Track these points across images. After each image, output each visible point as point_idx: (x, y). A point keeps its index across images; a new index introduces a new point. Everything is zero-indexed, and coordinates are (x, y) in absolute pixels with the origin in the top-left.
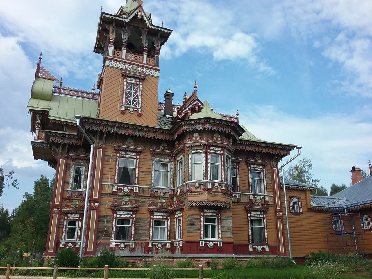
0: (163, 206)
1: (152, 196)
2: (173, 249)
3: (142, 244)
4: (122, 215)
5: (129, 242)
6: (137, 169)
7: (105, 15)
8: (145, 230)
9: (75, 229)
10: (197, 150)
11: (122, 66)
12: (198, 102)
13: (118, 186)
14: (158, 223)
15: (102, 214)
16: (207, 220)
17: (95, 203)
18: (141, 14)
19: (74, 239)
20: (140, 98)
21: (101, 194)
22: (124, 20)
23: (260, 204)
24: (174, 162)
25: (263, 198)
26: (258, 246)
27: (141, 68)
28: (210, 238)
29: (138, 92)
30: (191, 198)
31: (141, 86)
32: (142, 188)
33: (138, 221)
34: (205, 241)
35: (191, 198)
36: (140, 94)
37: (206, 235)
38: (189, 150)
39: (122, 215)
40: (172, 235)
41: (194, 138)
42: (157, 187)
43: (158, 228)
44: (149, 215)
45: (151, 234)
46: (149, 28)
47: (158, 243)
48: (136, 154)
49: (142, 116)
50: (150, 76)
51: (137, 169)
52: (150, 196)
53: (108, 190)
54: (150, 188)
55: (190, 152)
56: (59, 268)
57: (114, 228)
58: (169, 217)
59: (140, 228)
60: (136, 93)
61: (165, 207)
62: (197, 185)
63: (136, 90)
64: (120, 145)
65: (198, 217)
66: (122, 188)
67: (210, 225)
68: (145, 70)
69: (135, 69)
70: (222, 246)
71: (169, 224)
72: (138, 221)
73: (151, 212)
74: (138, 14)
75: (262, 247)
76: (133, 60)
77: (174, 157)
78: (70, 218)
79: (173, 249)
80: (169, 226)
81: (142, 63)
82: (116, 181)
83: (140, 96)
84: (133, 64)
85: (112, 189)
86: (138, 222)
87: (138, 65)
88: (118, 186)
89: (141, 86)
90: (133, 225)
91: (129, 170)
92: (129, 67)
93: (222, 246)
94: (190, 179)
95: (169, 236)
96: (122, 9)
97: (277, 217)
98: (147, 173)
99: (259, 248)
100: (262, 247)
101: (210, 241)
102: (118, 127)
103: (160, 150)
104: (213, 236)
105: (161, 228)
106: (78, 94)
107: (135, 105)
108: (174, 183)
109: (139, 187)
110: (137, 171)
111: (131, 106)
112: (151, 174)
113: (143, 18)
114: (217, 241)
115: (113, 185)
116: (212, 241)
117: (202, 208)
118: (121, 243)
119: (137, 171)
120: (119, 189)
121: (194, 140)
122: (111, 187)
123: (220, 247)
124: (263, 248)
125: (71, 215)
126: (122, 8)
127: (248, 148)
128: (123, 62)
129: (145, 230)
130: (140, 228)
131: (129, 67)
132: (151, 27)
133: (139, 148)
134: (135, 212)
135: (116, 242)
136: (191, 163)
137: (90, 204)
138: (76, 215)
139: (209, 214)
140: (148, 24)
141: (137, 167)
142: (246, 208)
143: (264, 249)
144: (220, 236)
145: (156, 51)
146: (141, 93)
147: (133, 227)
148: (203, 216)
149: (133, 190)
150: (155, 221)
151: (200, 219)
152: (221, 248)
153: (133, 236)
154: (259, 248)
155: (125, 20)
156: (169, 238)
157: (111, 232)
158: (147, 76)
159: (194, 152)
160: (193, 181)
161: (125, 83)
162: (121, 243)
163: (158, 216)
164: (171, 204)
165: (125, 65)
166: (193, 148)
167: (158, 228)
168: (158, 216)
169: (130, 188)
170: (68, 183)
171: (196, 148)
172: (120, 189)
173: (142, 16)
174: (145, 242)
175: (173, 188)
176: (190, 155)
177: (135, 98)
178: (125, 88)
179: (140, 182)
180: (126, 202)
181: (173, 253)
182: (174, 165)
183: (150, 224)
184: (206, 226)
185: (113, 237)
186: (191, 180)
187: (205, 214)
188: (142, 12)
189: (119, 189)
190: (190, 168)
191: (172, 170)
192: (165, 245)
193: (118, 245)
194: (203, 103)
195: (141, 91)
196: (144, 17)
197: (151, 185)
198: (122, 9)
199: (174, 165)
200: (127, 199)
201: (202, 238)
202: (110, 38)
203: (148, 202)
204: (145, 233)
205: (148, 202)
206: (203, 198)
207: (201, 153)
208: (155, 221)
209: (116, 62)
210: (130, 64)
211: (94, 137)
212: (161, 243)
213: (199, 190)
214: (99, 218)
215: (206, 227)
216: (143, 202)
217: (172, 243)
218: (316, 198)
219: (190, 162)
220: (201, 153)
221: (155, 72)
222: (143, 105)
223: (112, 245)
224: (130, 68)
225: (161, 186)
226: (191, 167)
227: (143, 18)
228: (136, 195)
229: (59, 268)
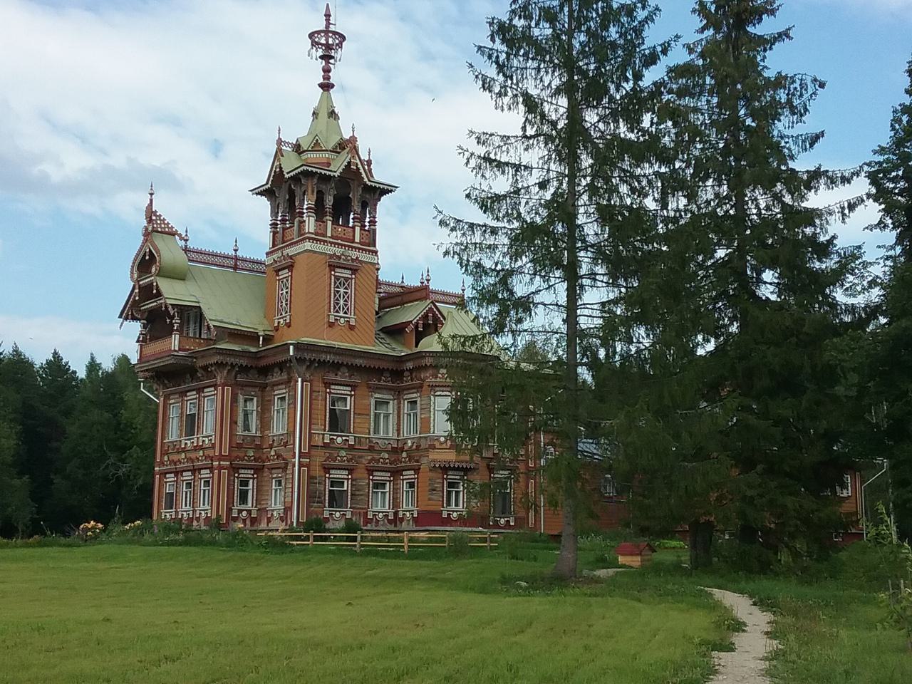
1: (371, 449)
2: (396, 520)
3: (360, 513)
4: (337, 474)
5: (345, 511)
6: (352, 410)
8: (361, 495)
9: (247, 491)
10: (443, 391)
11: (330, 250)
12: (433, 307)
13: (330, 435)
14: (376, 486)
15: (313, 473)
16: (451, 485)
19: (247, 505)
21: (311, 447)
22: (332, 174)
23: (508, 460)
24: (398, 399)
25: (347, 321)
26: (501, 518)
28: (453, 507)
29: (349, 291)
30: (433, 455)
31: (353, 281)
32: (358, 437)
33: (354, 483)
34: (448, 511)
35: (433, 455)
37: (449, 504)
38: (431, 390)
39: (337, 474)
40: (396, 503)
41: (440, 375)
42: (376, 436)
43: (377, 492)
44: (367, 476)
45: (370, 500)
46: (365, 184)
47: (379, 512)
48: (350, 389)
49: (356, 330)
51: (352, 410)
52: (369, 449)
53: (318, 441)
54: (369, 438)
55: (432, 393)
56: (315, 534)
57: (327, 493)
58: (392, 479)
59: (357, 493)
60: (346, 293)
61: (388, 465)
62: (442, 439)
63: (346, 288)
64: (331, 377)
65: (440, 481)
66: (335, 437)
71: (392, 487)
72: (354, 483)
73: (370, 471)
75: (506, 519)
77: (399, 392)
78: (242, 476)
79: (396, 520)
80: (392, 490)
81: (353, 241)
82: (327, 429)
85: (323, 439)
86: (355, 485)
88: (330, 435)
89: (353, 281)
90: (350, 488)
91: (337, 412)
92: (338, 251)
94: (432, 430)
95: (391, 504)
96: (317, 141)
98: (363, 417)
99: (502, 521)
100: (506, 519)
101: (453, 511)
102: (335, 354)
103: (382, 383)
104: (457, 505)
105: (382, 492)
106: (207, 258)
107: (345, 313)
108: (398, 430)
109: (355, 437)
110: (352, 413)
111: (341, 314)
112: (368, 417)
113: (358, 169)
114: (388, 512)
115: (323, 434)
116: (456, 511)
117: (445, 469)
118: (336, 511)
119: (352, 413)
120: (331, 439)
121: (440, 378)
122: (321, 436)
124: (507, 521)
125: (243, 471)
126: (317, 138)
128: (330, 242)
129: (361, 495)
130: (357, 493)
131: (338, 251)
132: (369, 183)
133: (355, 380)
134: (351, 471)
135: (330, 511)
136: (434, 409)
138: (249, 471)
139: (453, 476)
140: (366, 180)
141: (352, 407)
142: (488, 465)
143: (508, 521)
147: (349, 491)
148: (447, 479)
151: (443, 483)
153: (349, 502)
154: (502, 521)
155: (334, 174)
156: (391, 507)
157: (323, 498)
159: (438, 393)
160: (437, 433)
161: (333, 277)
162: (336, 511)
163: (379, 476)
164: (395, 460)
166: (437, 389)
167: (377, 492)
168: (379, 476)
169: (344, 438)
170: (236, 423)
171: (442, 389)
172: (332, 439)
174: (364, 511)
175: (396, 438)
176: (432, 398)
177: (346, 301)
178: (332, 286)
179: (356, 429)
181: (395, 526)
182: (399, 403)
183: (369, 487)
184: (449, 491)
185: (327, 505)
186: (434, 433)
187: (449, 477)
189: (331, 439)
190: (432, 416)
191: (396, 412)
192: (387, 516)
193: (332, 514)
194: (445, 315)
195: (353, 290)
196: (360, 166)
197: (369, 434)
198: (317, 141)
199: (399, 403)
200: (343, 453)
203: (366, 458)
204: (362, 499)
205: (366, 458)
206: (451, 456)
207: (449, 396)
209: (313, 242)
212: (382, 512)
213: (444, 446)
214: (311, 478)
215: (449, 493)
216: (361, 457)
217: (396, 514)
218: (590, 453)
219: (432, 408)
220: (449, 396)
222: (357, 312)
223: (326, 515)
225: (381, 435)
226: (434, 415)
228: (351, 448)
229: (315, 534)
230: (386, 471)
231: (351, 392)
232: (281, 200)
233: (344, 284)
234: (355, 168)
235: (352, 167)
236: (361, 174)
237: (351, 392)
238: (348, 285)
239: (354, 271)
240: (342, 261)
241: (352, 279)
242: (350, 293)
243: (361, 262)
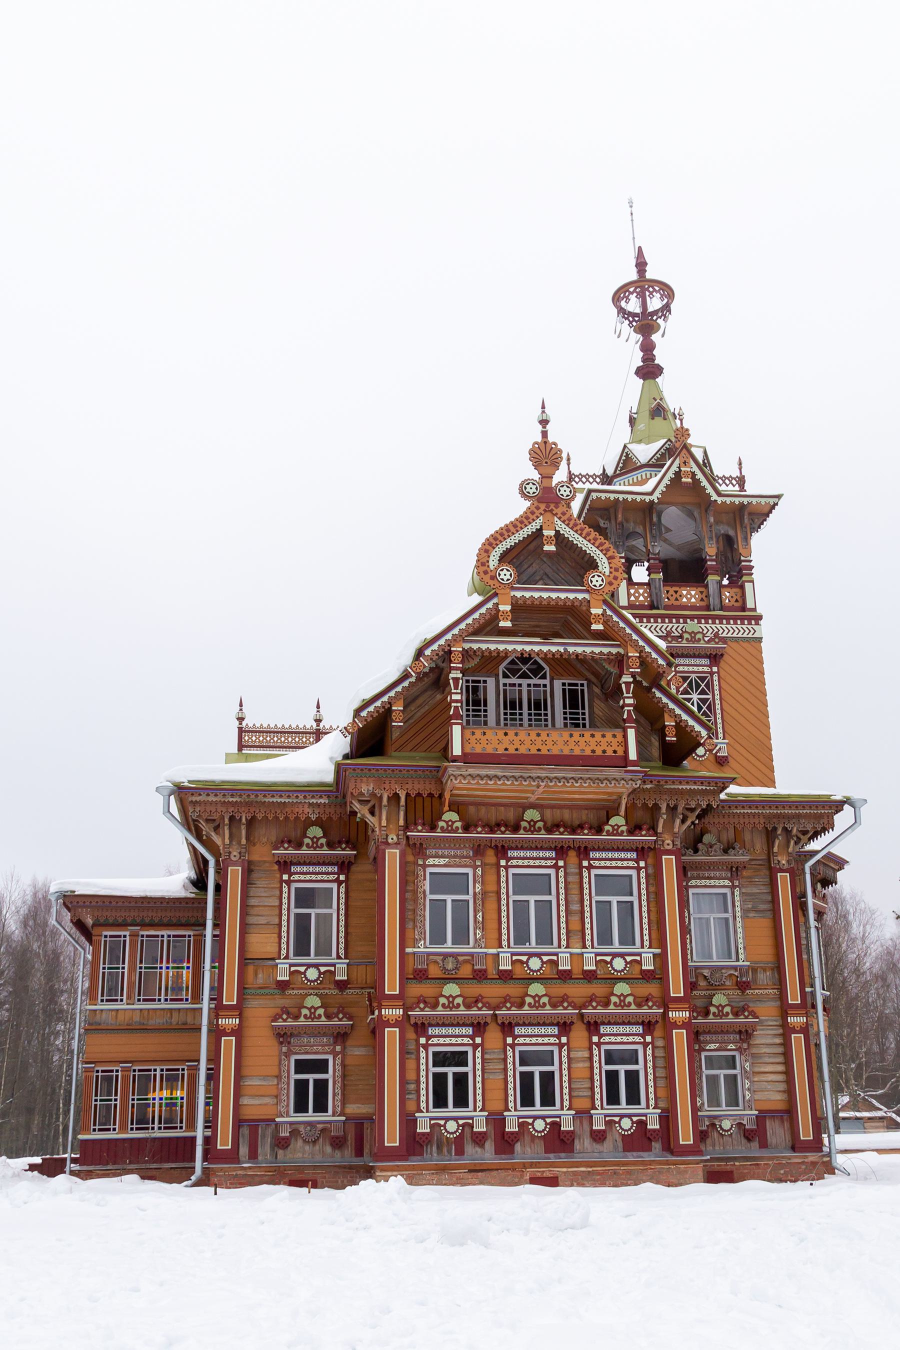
0: (725, 1016)
7: (599, 495)
17: (230, 1020)
18: (689, 469)
20: (718, 711)
27: (708, 623)
31: (715, 678)
36: (718, 702)
48: (470, 1031)
50: (736, 640)
58: (342, 877)
60: (704, 701)
63: (703, 692)
67: (622, 1069)
68: (718, 626)
69: (693, 632)
70: (658, 1127)
74: (680, 470)
76: (731, 604)
83: (718, 707)
84: (685, 617)
87: (699, 618)
89: (715, 678)
93: (658, 1127)
97: (787, 1031)
109: (571, 954)
113: (696, 482)
123: (654, 1130)
127: (333, 812)
137: (217, 1021)
144: (566, 1103)
145: (709, 563)
146: (717, 697)
149: (333, 973)
150: (296, 1060)
152: (426, 1136)
158: (725, 643)
165: (665, 625)
173: (693, 474)
180: (313, 1010)
188: (692, 463)
195: (717, 692)
196: (699, 476)
201: (425, 1111)
202: (742, 558)
208: (296, 1060)
210: (678, 617)
211: (217, 834)
221: (707, 625)
224: (679, 629)
227: (699, 481)
230: (329, 864)
231: (559, 1038)
232: (420, 684)
233: (698, 686)
234: (690, 480)
235: (683, 480)
236: (704, 488)
237: (559, 1038)
238: (707, 685)
239: (715, 658)
240: (684, 644)
241: (712, 673)
242: (713, 720)
243: (724, 640)
